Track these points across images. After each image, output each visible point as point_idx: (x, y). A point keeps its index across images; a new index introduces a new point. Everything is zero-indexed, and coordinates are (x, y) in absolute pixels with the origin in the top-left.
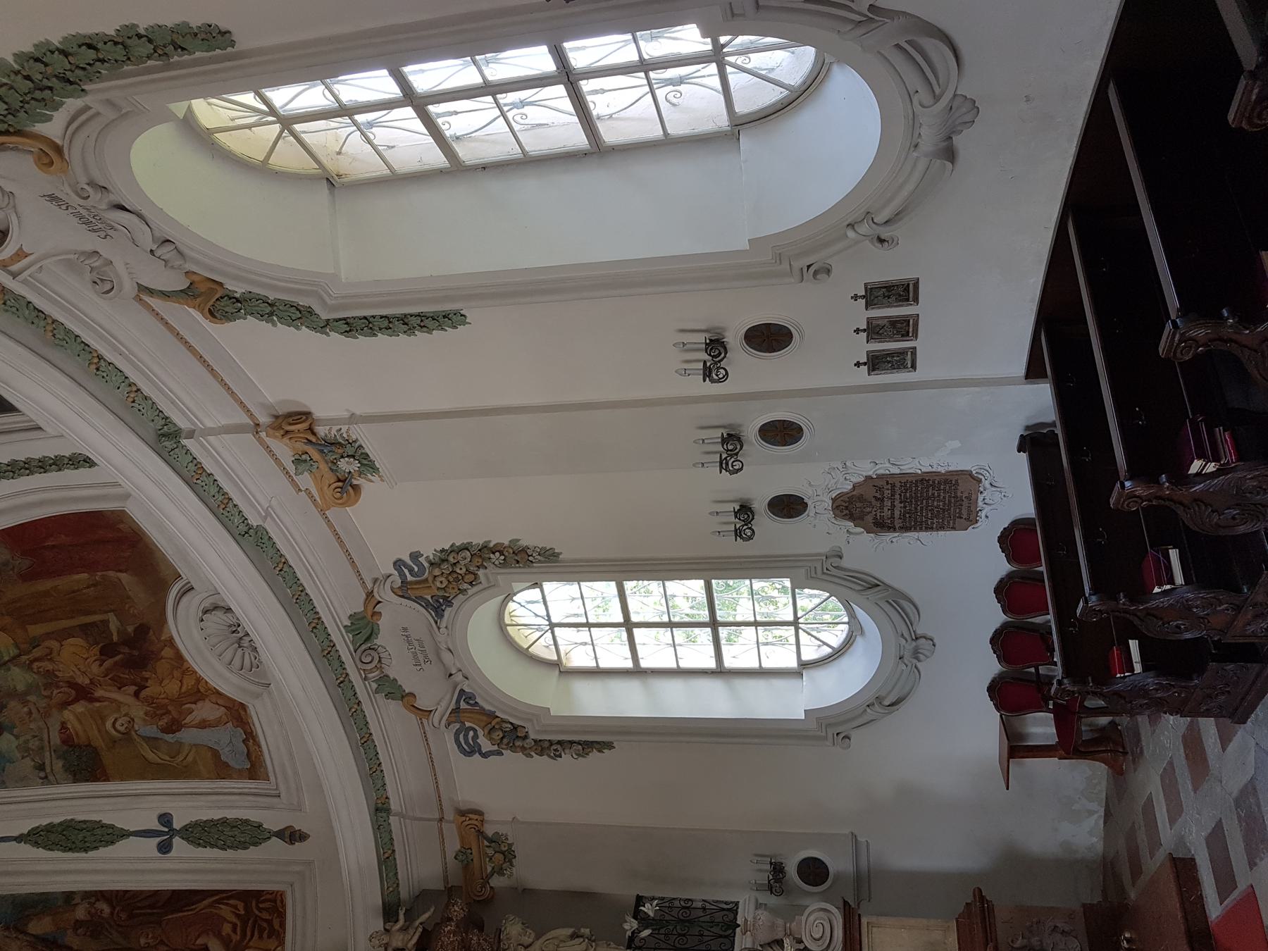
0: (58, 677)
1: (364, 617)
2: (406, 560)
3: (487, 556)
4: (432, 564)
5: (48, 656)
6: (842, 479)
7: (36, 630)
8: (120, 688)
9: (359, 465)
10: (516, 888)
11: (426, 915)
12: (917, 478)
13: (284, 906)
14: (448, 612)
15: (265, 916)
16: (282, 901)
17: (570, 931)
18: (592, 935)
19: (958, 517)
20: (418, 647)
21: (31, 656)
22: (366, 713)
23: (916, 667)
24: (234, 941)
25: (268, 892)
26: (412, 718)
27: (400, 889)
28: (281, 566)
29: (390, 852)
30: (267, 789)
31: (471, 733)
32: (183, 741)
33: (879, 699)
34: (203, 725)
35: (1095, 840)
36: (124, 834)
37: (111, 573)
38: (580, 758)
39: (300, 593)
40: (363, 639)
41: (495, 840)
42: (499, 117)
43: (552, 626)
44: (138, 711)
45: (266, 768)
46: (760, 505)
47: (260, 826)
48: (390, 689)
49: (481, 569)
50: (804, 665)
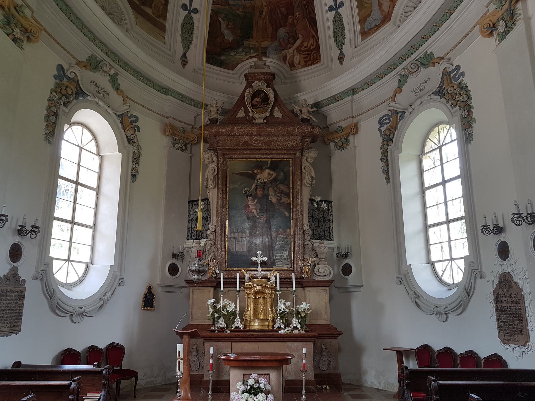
1: (431, 59)
2: (460, 70)
3: (466, 109)
4: (460, 83)
6: (520, 277)
9: (502, 31)
10: (330, 153)
11: (314, 119)
12: (523, 315)
13: (316, 63)
14: (438, 97)
16: (317, 62)
17: (314, 176)
18: (313, 185)
19: (505, 334)
20: (422, 88)
22: (391, 73)
23: (434, 313)
25: (320, 56)
28: (449, 12)
29: (338, 99)
31: (388, 121)
33: (418, 297)
35: (369, 383)
38: (382, 170)
39: (438, 25)
41: (347, 141)
43: (440, 148)
46: (503, 237)
47: (343, 44)
49: (459, 107)
50: (433, 265)
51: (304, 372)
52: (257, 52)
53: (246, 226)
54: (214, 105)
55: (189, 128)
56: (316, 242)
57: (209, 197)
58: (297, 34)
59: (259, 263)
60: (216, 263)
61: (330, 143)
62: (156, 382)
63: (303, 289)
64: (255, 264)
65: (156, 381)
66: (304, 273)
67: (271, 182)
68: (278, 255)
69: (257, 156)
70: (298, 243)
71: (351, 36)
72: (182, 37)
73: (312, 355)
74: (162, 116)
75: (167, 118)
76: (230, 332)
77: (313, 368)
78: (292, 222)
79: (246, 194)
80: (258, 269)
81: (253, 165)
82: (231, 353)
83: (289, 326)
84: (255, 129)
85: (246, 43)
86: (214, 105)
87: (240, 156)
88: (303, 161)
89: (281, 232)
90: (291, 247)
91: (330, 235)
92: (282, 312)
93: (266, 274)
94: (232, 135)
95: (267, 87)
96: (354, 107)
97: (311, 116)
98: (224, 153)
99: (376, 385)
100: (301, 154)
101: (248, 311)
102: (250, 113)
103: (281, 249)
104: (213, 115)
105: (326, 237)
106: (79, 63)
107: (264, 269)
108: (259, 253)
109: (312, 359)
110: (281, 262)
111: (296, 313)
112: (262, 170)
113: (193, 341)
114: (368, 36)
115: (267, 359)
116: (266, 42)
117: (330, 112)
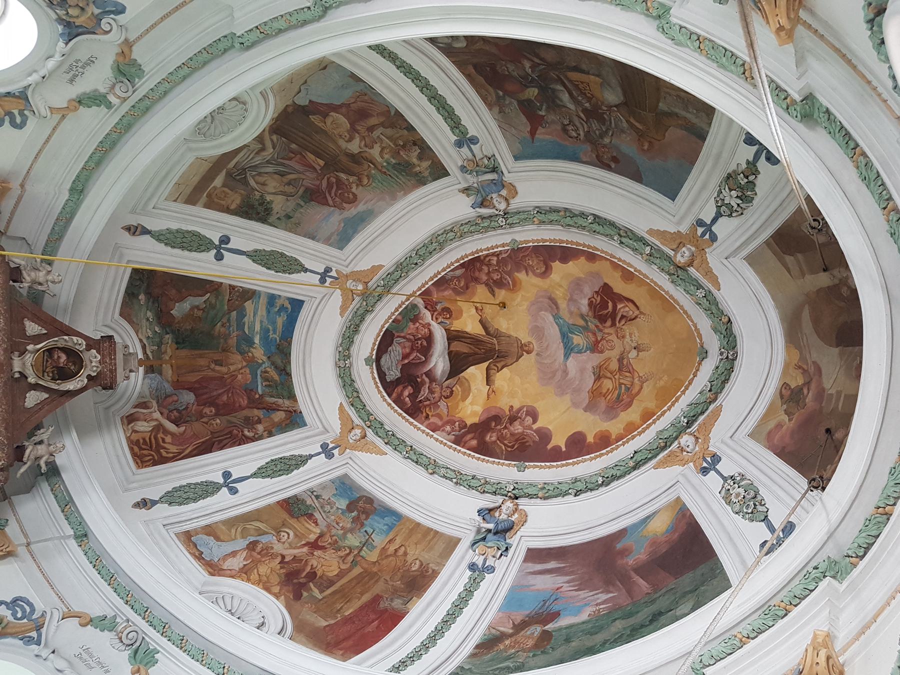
0: (333, 549)
5: (344, 558)
7: (357, 571)
8: (295, 556)
11: (22, 470)
13: (135, 460)
15: (145, 452)
16: (137, 463)
20: (91, 662)
21: (352, 555)
25: (149, 466)
26: (76, 608)
27: (49, 488)
29: (66, 510)
32: (242, 540)
34: (234, 554)
36: (254, 475)
37: (332, 622)
40: (140, 650)
42: (318, 273)
44: (278, 548)
45: (180, 540)
48: (103, 623)
54: (50, 278)
58: (185, 424)
72: (178, 231)
75: (22, 186)
85: (168, 338)
86: (50, 278)
96: (49, 543)
97: (29, 464)
102: (35, 345)
104: (29, 275)
106: (128, 44)
116: (170, 372)
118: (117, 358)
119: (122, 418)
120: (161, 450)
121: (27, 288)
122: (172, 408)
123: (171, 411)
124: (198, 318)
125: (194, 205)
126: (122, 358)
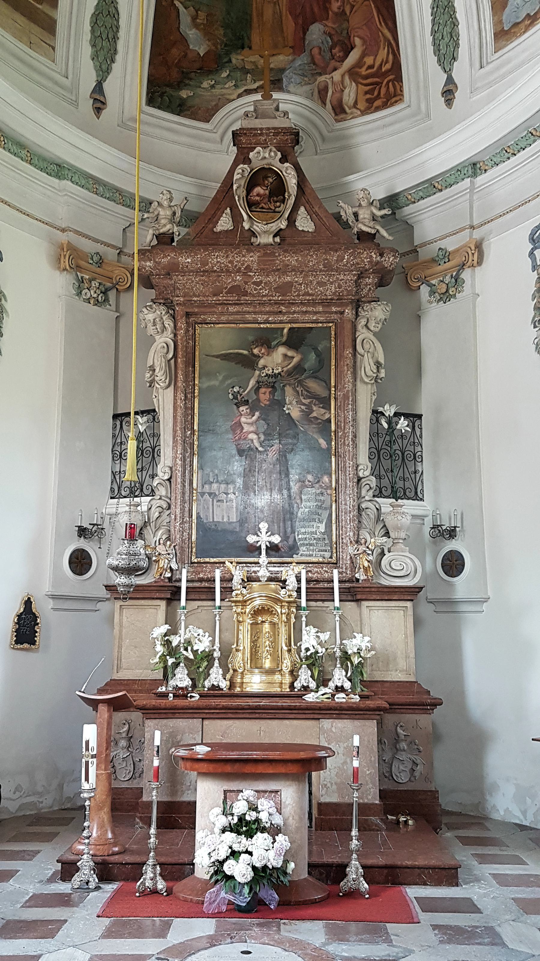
13: (392, 105)
16: (396, 102)
17: (382, 360)
18: (381, 379)
24: (360, 70)
25: (401, 87)
29: (440, 187)
30: (487, 54)
35: (502, 813)
38: (534, 346)
41: (457, 280)
47: (454, 59)
51: (355, 787)
52: (261, 80)
53: (235, 468)
54: (165, 203)
55: (111, 254)
56: (386, 504)
57: (156, 406)
58: (352, 38)
59: (263, 547)
60: (172, 547)
61: (419, 286)
62: (41, 805)
63: (358, 604)
64: (255, 550)
65: (42, 802)
66: (359, 570)
67: (290, 373)
68: (303, 530)
69: (260, 318)
70: (346, 504)
71: (472, 41)
72: (94, 46)
73: (376, 750)
74: (51, 226)
75: (63, 230)
76: (201, 696)
77: (377, 779)
78: (333, 459)
79: (236, 401)
80: (261, 561)
81: (251, 338)
82: (202, 744)
83: (326, 685)
84: (255, 258)
85: (236, 59)
86: (165, 203)
87: (223, 318)
88: (359, 327)
89: (310, 482)
90: (330, 515)
91: (416, 489)
92: (311, 654)
93: (277, 572)
94: (204, 271)
95: (282, 161)
96: (475, 205)
97: (378, 227)
98: (188, 310)
99: (517, 817)
100: (354, 313)
101: (237, 650)
102: (243, 220)
103: (310, 518)
104: (165, 225)
105: (407, 493)
107: (274, 560)
108: (264, 526)
109: (375, 758)
110: (311, 545)
111: (341, 657)
112: (271, 348)
113: (120, 716)
114: (509, 40)
115: (277, 757)
116: (281, 57)
117: (423, 217)
118: (260, 126)
119: (337, 121)
120: (383, 70)
121: (179, 228)
122: (328, 56)
123: (333, 57)
124: (209, 18)
125: (55, 22)
126: (261, 120)
